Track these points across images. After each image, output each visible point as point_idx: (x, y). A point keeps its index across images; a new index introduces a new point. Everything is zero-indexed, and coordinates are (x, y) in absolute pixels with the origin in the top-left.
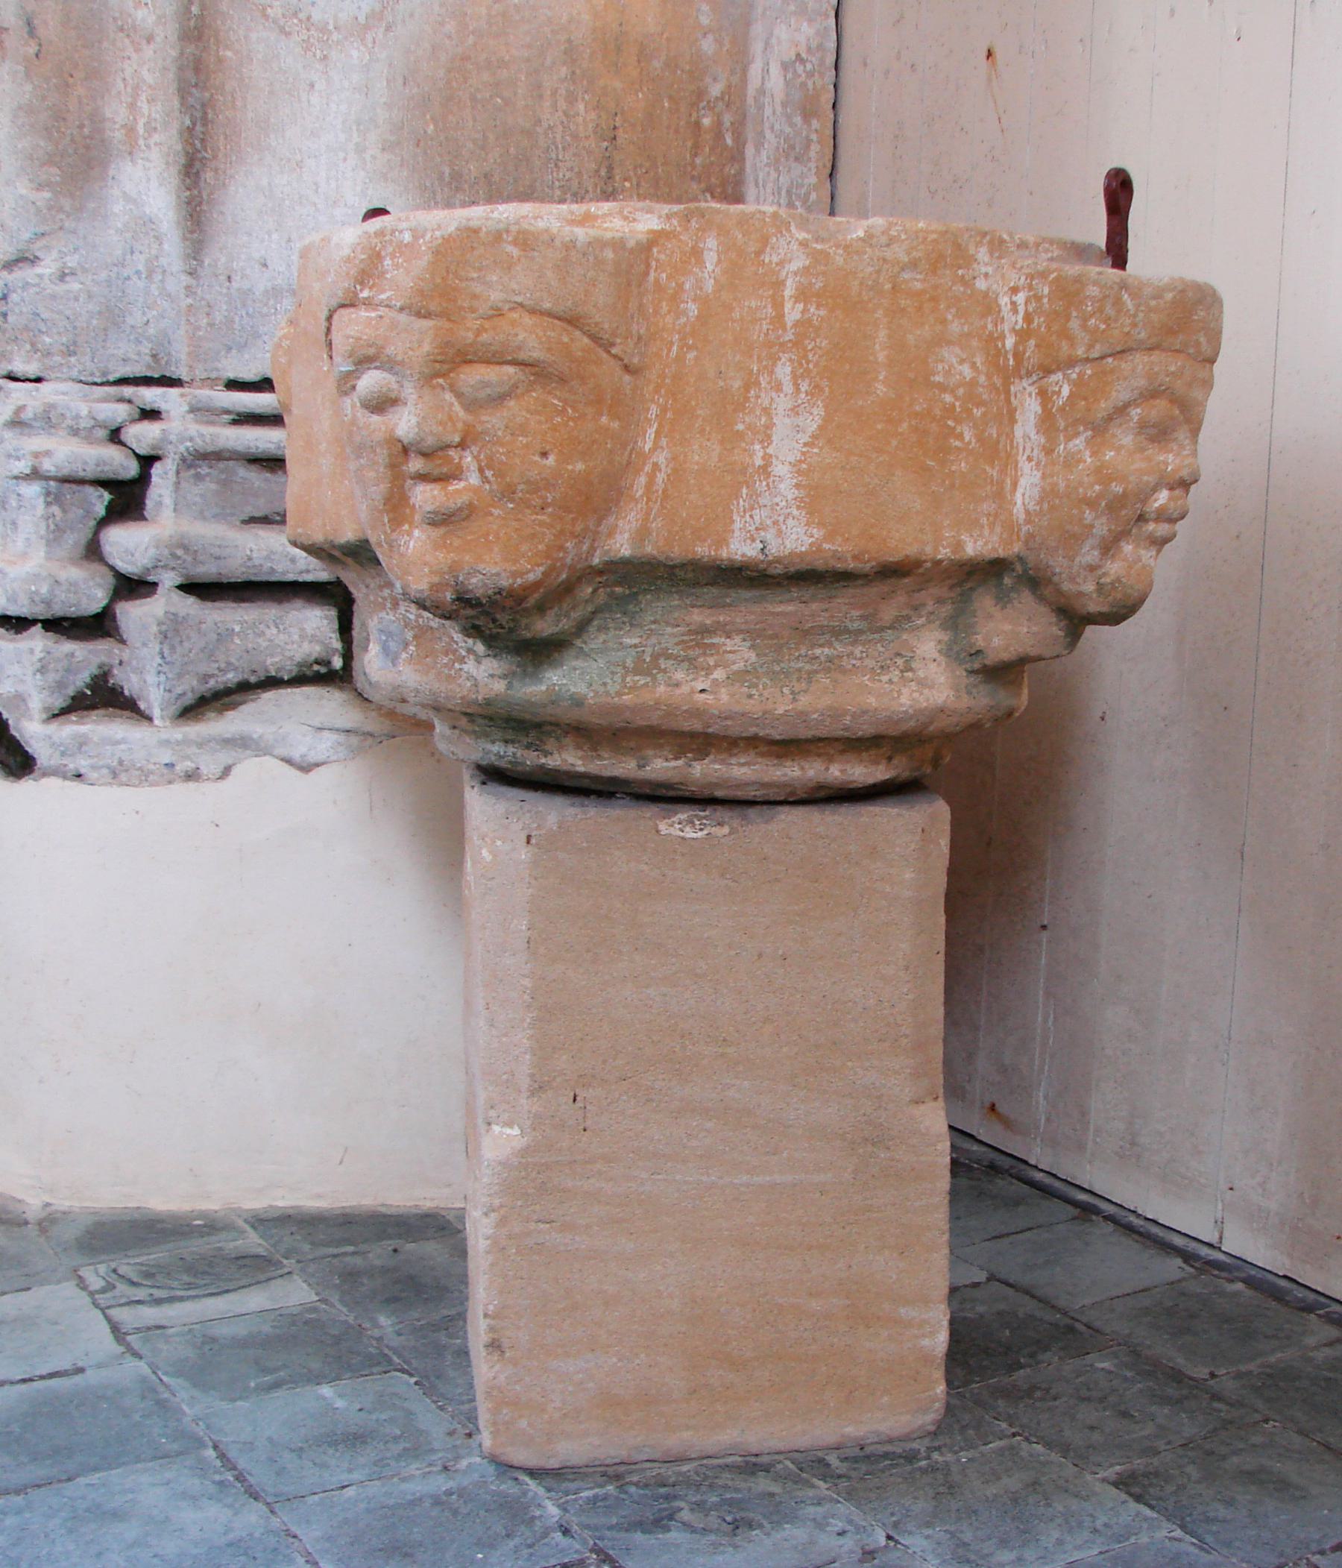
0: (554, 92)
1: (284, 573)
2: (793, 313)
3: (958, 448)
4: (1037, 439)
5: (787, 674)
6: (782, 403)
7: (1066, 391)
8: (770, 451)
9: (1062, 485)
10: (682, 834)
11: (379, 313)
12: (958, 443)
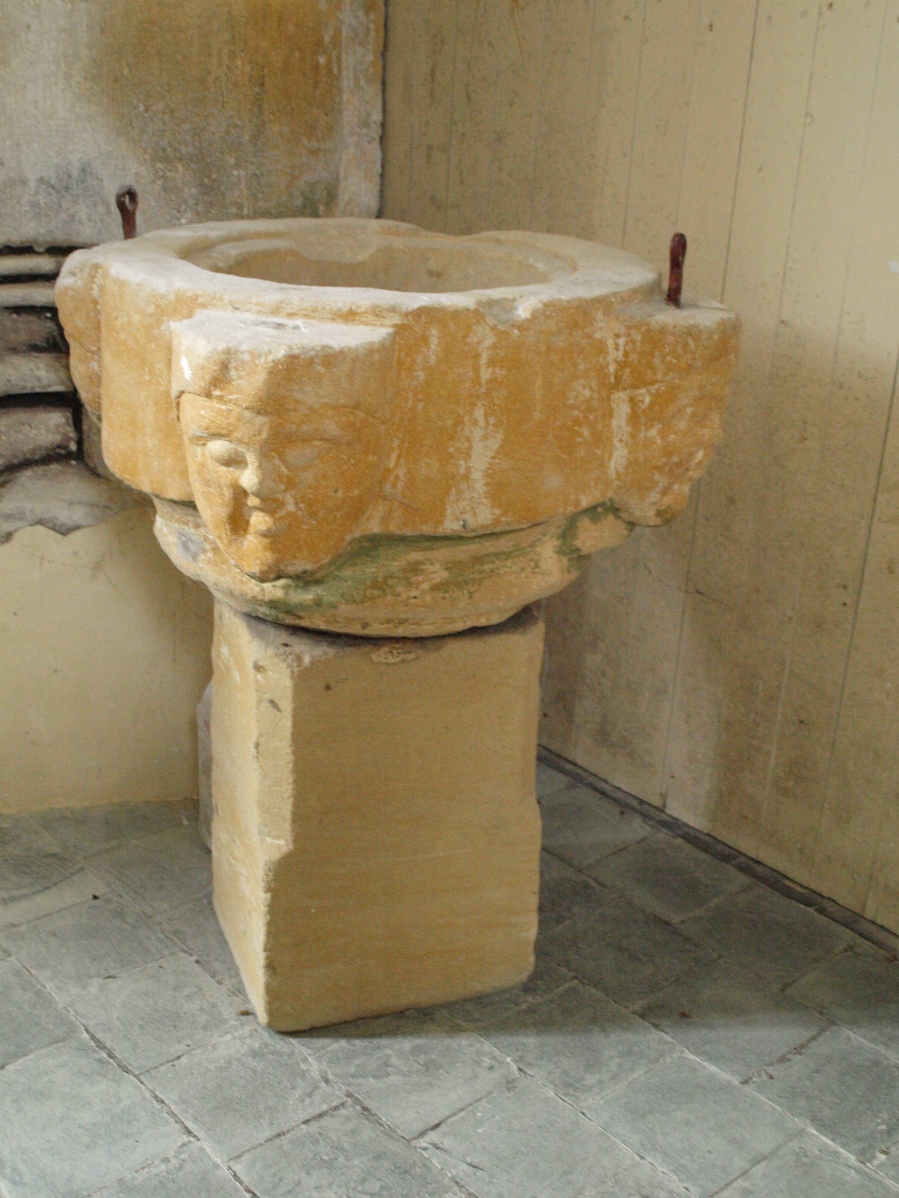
0: (220, 51)
1: (33, 388)
2: (486, 374)
3: (580, 443)
4: (627, 429)
5: (466, 582)
6: (478, 433)
7: (647, 400)
8: (470, 464)
9: (641, 459)
10: (386, 660)
11: (230, 408)
12: (580, 440)
